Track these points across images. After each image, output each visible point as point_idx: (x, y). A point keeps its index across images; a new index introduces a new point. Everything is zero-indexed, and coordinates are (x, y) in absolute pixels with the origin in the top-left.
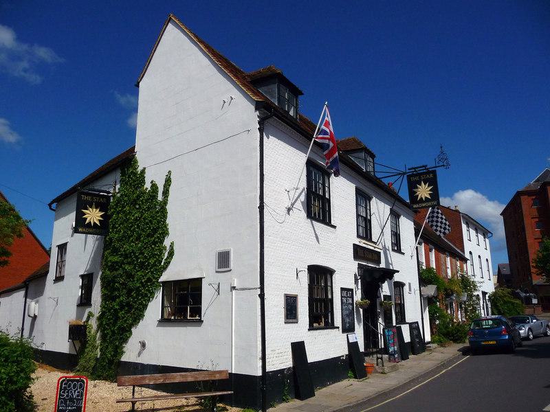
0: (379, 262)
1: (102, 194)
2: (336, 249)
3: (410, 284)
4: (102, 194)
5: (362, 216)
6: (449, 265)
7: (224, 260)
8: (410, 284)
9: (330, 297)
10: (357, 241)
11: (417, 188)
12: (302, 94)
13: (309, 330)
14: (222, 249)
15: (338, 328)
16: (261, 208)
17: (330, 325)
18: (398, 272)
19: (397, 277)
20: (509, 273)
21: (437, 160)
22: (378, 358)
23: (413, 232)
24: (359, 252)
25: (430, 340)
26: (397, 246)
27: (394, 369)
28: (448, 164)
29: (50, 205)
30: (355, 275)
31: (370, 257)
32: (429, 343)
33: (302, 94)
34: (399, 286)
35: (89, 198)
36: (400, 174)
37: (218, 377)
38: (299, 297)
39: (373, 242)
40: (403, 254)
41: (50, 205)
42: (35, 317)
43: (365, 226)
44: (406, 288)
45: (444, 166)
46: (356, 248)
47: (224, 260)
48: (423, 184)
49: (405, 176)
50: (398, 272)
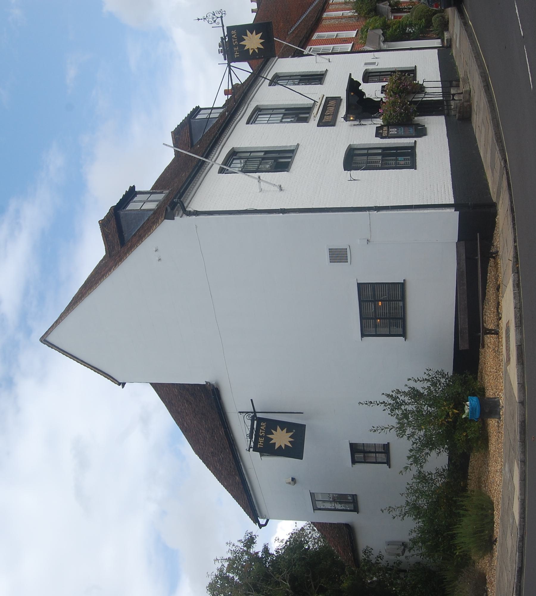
0: (338, 100)
1: (255, 427)
2: (322, 148)
3: (366, 64)
4: (255, 427)
5: (283, 118)
6: (340, 13)
7: (338, 256)
8: (366, 64)
9: (380, 151)
13: (416, 169)
15: (415, 141)
18: (350, 74)
19: (358, 77)
20: (464, 242)
21: (214, 25)
22: (453, 99)
23: (296, 59)
24: (327, 120)
25: (439, 40)
26: (317, 78)
27: (466, 80)
28: (220, 12)
29: (261, 526)
30: (351, 125)
31: (332, 109)
32: (443, 41)
34: (368, 76)
35: (261, 440)
36: (230, 73)
37: (463, 251)
39: (314, 104)
40: (298, 145)
41: (261, 526)
42: (354, 448)
44: (371, 67)
45: (222, 17)
46: (321, 124)
47: (338, 256)
49: (231, 64)
50: (350, 74)
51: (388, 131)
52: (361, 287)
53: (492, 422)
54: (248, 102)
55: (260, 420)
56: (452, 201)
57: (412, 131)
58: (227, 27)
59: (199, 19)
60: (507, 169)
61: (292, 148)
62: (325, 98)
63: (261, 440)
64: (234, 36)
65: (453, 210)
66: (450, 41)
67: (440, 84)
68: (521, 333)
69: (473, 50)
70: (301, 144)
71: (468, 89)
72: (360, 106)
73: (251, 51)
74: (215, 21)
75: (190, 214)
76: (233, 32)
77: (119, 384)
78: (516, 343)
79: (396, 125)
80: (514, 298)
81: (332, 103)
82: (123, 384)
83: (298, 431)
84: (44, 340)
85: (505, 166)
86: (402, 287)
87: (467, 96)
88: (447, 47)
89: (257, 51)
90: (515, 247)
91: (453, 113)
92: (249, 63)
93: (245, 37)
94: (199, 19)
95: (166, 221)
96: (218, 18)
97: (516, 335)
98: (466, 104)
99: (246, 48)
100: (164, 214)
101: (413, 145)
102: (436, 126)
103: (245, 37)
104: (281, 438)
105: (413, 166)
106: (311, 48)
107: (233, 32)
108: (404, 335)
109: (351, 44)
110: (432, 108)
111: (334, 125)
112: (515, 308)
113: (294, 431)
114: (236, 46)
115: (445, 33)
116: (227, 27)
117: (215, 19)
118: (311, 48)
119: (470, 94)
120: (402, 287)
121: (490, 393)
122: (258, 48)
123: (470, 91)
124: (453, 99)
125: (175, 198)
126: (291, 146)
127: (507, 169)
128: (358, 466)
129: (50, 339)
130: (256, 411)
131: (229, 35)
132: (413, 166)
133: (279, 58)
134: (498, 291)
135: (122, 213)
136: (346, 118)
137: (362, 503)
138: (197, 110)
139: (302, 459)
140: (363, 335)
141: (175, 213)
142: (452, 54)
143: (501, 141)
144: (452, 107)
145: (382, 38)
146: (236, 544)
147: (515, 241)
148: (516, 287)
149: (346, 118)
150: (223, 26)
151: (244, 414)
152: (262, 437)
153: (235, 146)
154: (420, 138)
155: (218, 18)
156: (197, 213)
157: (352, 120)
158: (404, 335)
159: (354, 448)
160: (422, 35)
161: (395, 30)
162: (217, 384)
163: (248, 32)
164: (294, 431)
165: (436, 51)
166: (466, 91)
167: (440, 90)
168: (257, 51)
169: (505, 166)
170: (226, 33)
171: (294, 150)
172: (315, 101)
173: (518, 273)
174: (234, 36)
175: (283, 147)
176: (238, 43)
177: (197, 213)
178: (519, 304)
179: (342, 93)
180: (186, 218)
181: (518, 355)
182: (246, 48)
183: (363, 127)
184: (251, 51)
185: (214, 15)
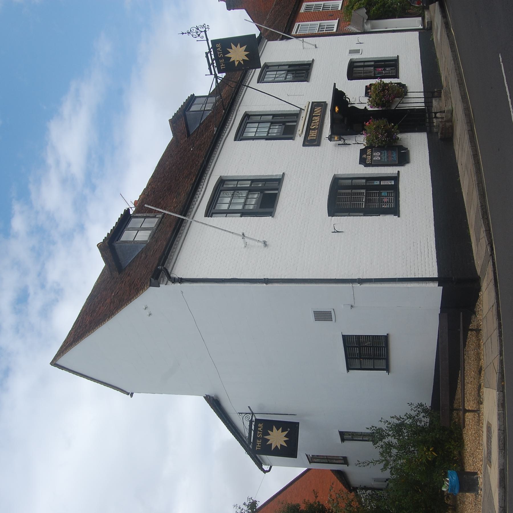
0: (322, 105)
1: (253, 428)
3: (351, 52)
4: (253, 428)
5: (270, 126)
7: (323, 316)
10: (299, 139)
11: (269, 434)
12: (399, 216)
14: (312, 317)
15: (399, 172)
16: (267, 281)
17: (396, 178)
18: (335, 84)
21: (199, 38)
22: (436, 117)
23: (284, 42)
25: (420, 19)
32: (423, 19)
33: (399, 216)
38: (269, 219)
41: (265, 472)
42: (343, 435)
43: (283, 125)
44: (356, 57)
45: (205, 31)
46: (308, 142)
47: (323, 316)
48: (273, 447)
50: (335, 84)
51: (372, 155)
52: (346, 339)
53: (470, 496)
54: (237, 108)
55: (258, 421)
56: (436, 276)
57: (395, 156)
58: (211, 41)
59: (183, 33)
60: (493, 259)
61: (278, 177)
62: (311, 103)
63: (259, 442)
64: (219, 49)
65: (436, 284)
66: (431, 23)
67: (422, 95)
68: (504, 457)
69: (456, 70)
70: (286, 173)
71: (450, 107)
72: (346, 119)
73: (236, 63)
74: (199, 35)
75: (175, 281)
76: (218, 45)
77: (128, 394)
78: (499, 467)
79: (380, 148)
80: (499, 419)
81: (318, 110)
82: (132, 395)
83: (291, 429)
84: (54, 363)
85: (492, 255)
86: (386, 338)
87: (449, 115)
88: (427, 29)
89: (242, 62)
90: (501, 362)
91: (435, 130)
92: (246, 10)
93: (230, 50)
94: (183, 33)
95: (151, 288)
96: (201, 32)
97: (499, 459)
98: (448, 124)
99: (231, 60)
100: (149, 283)
101: (396, 175)
102: (417, 144)
103: (230, 50)
104: (277, 438)
105: (395, 211)
106: (299, 25)
107: (218, 45)
108: (387, 369)
109: (337, 21)
110: (416, 121)
111: (319, 145)
112: (499, 430)
113: (289, 429)
114: (221, 58)
115: (426, 13)
116: (211, 41)
117: (199, 33)
118: (299, 25)
119: (452, 114)
120: (386, 338)
121: (469, 469)
122: (243, 60)
123: (453, 111)
124: (436, 117)
125: (158, 265)
126: (276, 175)
127: (493, 259)
128: (346, 443)
129: (60, 362)
130: (254, 412)
131: (214, 47)
132: (395, 211)
133: (268, 41)
134: (480, 375)
135: (116, 245)
136: (330, 138)
137: (350, 460)
138: (192, 99)
139: (296, 457)
140: (349, 369)
141: (160, 281)
142: (433, 39)
143: (487, 218)
144: (435, 124)
145: (367, 17)
146: (242, 508)
147: (501, 354)
148: (500, 407)
149: (330, 138)
150: (207, 40)
151: (243, 415)
152: (259, 439)
153: (223, 175)
154: (402, 167)
155: (201, 32)
156: (181, 281)
157: (337, 141)
158: (387, 369)
159: (343, 435)
160: (404, 14)
161: (379, 9)
162: (217, 397)
163: (233, 46)
164: (289, 429)
165: (417, 33)
166: (448, 111)
167: (423, 100)
168: (242, 62)
169: (492, 255)
170: (211, 46)
171: (280, 179)
172: (301, 109)
173: (503, 391)
174: (219, 49)
175: (269, 176)
176: (224, 55)
177: (181, 281)
178: (503, 427)
179: (328, 99)
180: (171, 287)
181: (500, 479)
182: (231, 60)
183: (346, 148)
184: (236, 63)
185: (198, 29)
